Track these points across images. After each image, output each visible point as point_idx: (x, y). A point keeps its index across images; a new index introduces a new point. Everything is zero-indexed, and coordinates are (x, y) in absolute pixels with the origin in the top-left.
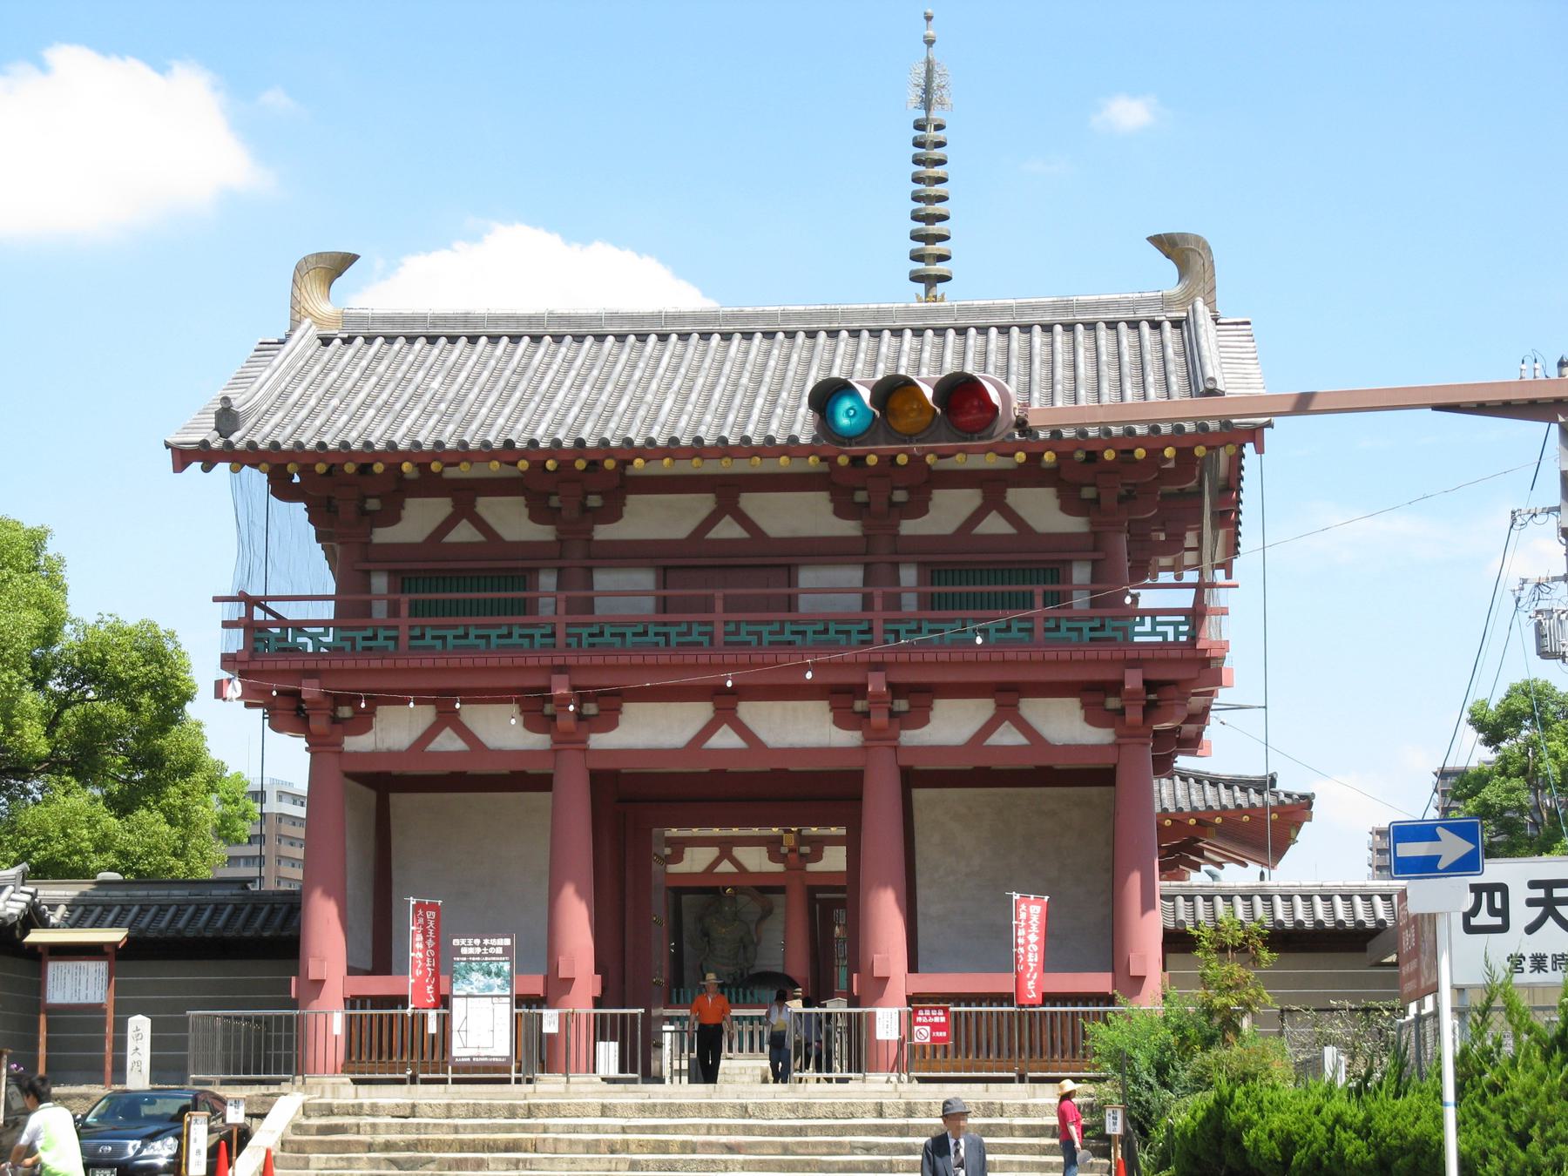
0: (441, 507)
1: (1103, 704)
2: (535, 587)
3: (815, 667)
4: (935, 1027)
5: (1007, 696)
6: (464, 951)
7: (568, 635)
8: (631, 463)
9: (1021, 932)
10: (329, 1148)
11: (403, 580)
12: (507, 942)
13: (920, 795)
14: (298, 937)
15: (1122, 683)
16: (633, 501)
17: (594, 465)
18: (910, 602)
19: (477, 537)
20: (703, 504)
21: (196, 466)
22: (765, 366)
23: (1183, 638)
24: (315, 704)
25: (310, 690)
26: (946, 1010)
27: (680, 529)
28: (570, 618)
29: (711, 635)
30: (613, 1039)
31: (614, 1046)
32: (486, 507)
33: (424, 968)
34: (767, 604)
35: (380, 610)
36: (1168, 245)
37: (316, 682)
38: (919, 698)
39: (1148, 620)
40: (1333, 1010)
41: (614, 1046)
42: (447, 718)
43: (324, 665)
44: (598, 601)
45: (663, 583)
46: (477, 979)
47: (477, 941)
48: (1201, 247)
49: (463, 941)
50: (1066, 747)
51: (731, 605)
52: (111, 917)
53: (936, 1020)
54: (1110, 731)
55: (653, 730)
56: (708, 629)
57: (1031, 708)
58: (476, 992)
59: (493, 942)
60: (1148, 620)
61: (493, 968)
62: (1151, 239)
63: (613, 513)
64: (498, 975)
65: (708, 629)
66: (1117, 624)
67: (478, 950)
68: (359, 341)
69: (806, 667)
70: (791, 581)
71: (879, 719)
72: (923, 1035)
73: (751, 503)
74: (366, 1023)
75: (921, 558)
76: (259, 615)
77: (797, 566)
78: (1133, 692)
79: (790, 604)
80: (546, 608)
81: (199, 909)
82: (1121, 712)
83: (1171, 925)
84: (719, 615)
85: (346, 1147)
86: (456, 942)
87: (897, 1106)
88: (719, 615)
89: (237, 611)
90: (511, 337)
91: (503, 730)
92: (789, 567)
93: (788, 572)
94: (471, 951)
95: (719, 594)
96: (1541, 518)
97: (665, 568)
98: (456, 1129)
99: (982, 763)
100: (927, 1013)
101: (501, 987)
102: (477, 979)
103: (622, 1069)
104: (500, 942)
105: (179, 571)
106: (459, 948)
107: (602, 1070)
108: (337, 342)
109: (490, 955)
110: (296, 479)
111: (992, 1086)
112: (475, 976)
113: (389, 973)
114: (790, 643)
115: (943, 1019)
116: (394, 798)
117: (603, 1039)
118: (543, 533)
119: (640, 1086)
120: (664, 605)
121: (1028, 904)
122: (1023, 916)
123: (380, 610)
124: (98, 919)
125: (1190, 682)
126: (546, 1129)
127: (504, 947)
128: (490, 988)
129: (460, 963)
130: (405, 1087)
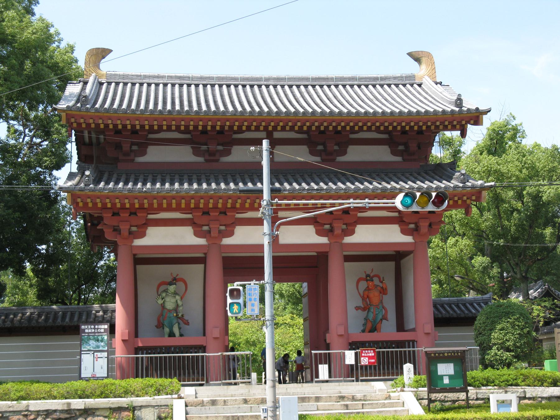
4: (370, 358)
6: (87, 331)
12: (106, 327)
13: (139, 267)
26: (374, 350)
30: (325, 363)
31: (326, 367)
41: (326, 367)
46: (93, 343)
47: (93, 327)
48: (429, 55)
49: (86, 327)
53: (370, 355)
54: (205, 239)
58: (92, 349)
59: (100, 327)
61: (100, 338)
64: (102, 341)
67: (93, 330)
71: (214, 233)
72: (364, 361)
82: (209, 232)
86: (83, 327)
94: (90, 331)
100: (367, 351)
103: (330, 376)
104: (103, 327)
106: (84, 330)
115: (373, 354)
117: (321, 363)
119: (355, 383)
127: (105, 329)
128: (98, 347)
129: (85, 336)
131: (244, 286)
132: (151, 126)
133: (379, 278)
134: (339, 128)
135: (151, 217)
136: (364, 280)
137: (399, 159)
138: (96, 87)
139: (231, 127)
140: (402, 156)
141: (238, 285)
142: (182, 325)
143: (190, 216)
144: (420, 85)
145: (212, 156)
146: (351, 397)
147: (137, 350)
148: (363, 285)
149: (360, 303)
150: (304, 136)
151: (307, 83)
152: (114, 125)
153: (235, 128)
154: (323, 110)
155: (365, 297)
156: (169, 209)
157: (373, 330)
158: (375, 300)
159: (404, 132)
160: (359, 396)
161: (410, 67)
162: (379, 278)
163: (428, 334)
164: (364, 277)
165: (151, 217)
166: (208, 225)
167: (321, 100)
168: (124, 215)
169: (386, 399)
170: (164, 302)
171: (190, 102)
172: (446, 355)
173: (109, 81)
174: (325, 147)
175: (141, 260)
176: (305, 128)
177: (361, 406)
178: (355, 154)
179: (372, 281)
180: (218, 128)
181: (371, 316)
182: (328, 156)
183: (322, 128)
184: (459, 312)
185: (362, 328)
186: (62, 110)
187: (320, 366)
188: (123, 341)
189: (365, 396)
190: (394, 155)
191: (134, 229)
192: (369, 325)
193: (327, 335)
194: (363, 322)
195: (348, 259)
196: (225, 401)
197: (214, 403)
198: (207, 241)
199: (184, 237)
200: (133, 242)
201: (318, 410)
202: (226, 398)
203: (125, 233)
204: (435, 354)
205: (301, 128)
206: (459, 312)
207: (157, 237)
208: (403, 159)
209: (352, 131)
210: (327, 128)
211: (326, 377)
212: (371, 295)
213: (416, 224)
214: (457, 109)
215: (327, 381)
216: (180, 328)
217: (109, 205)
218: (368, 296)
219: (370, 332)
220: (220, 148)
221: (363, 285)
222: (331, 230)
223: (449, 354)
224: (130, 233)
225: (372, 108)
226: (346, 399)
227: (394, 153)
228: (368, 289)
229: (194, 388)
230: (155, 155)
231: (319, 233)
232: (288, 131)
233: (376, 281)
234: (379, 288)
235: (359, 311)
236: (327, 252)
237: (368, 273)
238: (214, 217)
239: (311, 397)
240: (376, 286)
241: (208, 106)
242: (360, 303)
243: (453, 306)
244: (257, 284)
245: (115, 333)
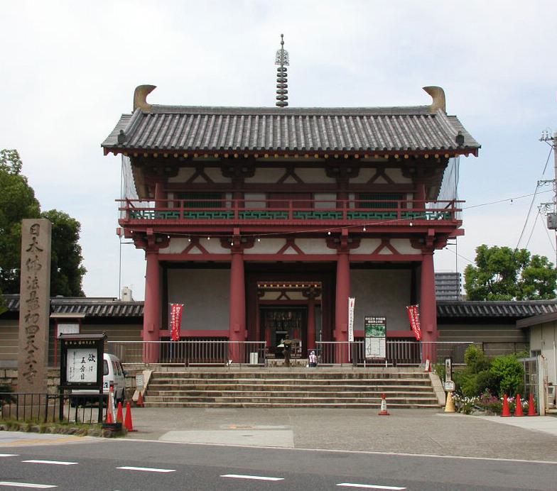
0: (192, 171)
1: (333, 241)
2: (225, 198)
3: (366, 227)
5: (290, 239)
6: (369, 322)
7: (348, 215)
8: (193, 156)
9: (173, 316)
10: (164, 388)
11: (179, 195)
15: (341, 233)
16: (258, 170)
17: (351, 157)
18: (352, 205)
19: (385, 182)
20: (282, 172)
21: (111, 154)
22: (184, 125)
23: (153, 218)
24: (150, 236)
25: (150, 232)
27: (274, 181)
28: (240, 209)
29: (288, 215)
32: (208, 171)
33: (175, 327)
34: (304, 205)
35: (171, 206)
36: (430, 90)
37: (152, 229)
38: (356, 238)
39: (435, 212)
42: (195, 242)
43: (155, 223)
44: (246, 204)
45: (268, 198)
46: (374, 331)
48: (441, 91)
50: (405, 255)
51: (295, 205)
52: (72, 310)
55: (265, 249)
56: (287, 213)
57: (394, 243)
59: (379, 319)
60: (435, 212)
61: (379, 328)
62: (425, 88)
63: (251, 174)
64: (381, 330)
65: (287, 213)
66: (270, 213)
68: (156, 115)
69: (363, 227)
70: (312, 197)
73: (298, 171)
74: (427, 345)
75: (176, 190)
76: (130, 206)
77: (315, 193)
78: (345, 237)
79: (312, 205)
80: (229, 205)
81: (102, 307)
83: (439, 316)
84: (291, 208)
85: (170, 388)
87: (356, 375)
88: (291, 208)
89: (119, 204)
91: (215, 248)
92: (311, 193)
93: (311, 195)
95: (291, 201)
96: (547, 183)
97: (270, 193)
98: (207, 382)
101: (382, 334)
102: (374, 331)
104: (382, 319)
105: (86, 188)
107: (252, 363)
108: (149, 115)
111: (201, 368)
112: (373, 331)
113: (438, 323)
114: (315, 218)
116: (169, 270)
118: (227, 180)
120: (269, 205)
121: (176, 307)
122: (174, 311)
123: (171, 206)
124: (67, 310)
125: (449, 233)
126: (238, 382)
130: (184, 368)
144: (433, 116)
161: (427, 101)
163: (430, 333)
170: (50, 314)
172: (80, 343)
187: (252, 354)
188: (150, 332)
193: (334, 331)
204: (69, 342)
211: (256, 363)
215: (256, 366)
223: (84, 343)
243: (459, 307)
245: (19, 319)
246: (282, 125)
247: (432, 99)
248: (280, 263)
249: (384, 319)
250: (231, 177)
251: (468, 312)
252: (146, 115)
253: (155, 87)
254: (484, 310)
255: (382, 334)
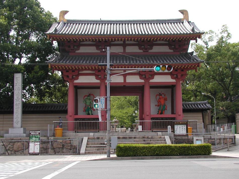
14: (23, 114)
40: (206, 87)
46: (34, 138)
54: (99, 80)
61: (37, 137)
62: (180, 11)
64: (38, 138)
67: (34, 133)
90: (73, 23)
94: (33, 134)
99: (188, 11)
101: (38, 140)
103: (142, 130)
104: (38, 132)
109: (36, 134)
110: (17, 54)
112: (34, 138)
127: (39, 133)
128: (36, 140)
131: (100, 98)
132: (112, 40)
133: (164, 94)
134: (180, 39)
135: (80, 72)
136: (158, 95)
137: (172, 51)
138: (62, 25)
139: (153, 39)
140: (173, 50)
141: (97, 98)
142: (92, 111)
143: (94, 72)
145: (146, 50)
146: (147, 137)
147: (76, 119)
148: (158, 97)
149: (157, 104)
150: (137, 43)
151: (171, 22)
152: (79, 40)
153: (155, 40)
154: (184, 33)
155: (159, 101)
156: (86, 69)
157: (162, 113)
158: (162, 103)
159: (70, 41)
160: (150, 137)
161: (181, 16)
162: (164, 94)
163: (148, 115)
164: (159, 94)
165: (80, 72)
166: (145, 75)
167: (159, 29)
168: (179, 71)
169: (160, 138)
171: (132, 32)
173: (68, 22)
174: (175, 46)
175: (77, 88)
176: (167, 40)
177: (150, 141)
178: (156, 49)
179: (161, 95)
180: (148, 40)
181: (161, 109)
182: (146, 50)
183: (174, 40)
184: (191, 107)
185: (158, 113)
186: (48, 34)
189: (152, 137)
190: (170, 49)
191: (74, 77)
192: (160, 111)
194: (158, 110)
195: (152, 87)
196: (102, 138)
197: (98, 138)
198: (144, 81)
199: (92, 80)
200: (74, 81)
201: (134, 141)
202: (102, 137)
203: (70, 77)
205: (166, 39)
206: (188, 107)
207: (82, 80)
208: (174, 51)
209: (156, 40)
210: (175, 39)
212: (161, 101)
213: (177, 75)
214: (192, 32)
216: (91, 112)
217: (97, 69)
218: (160, 101)
219: (160, 114)
220: (149, 47)
221: (158, 97)
222: (177, 77)
224: (73, 78)
225: (186, 32)
226: (145, 138)
227: (170, 49)
228: (160, 98)
229: (93, 133)
230: (83, 50)
231: (172, 78)
232: (88, 41)
233: (163, 95)
234: (164, 98)
235: (156, 106)
236: (100, 87)
237: (160, 93)
238: (100, 72)
239: (133, 137)
240: (163, 97)
241: (126, 32)
242: (157, 104)
243: (193, 105)
244: (104, 98)
245: (13, 114)
246: (128, 27)
247: (183, 15)
248: (124, 86)
249: (39, 132)
250: (100, 50)
251: (200, 107)
252: (65, 24)
253: (68, 11)
254: (203, 106)
255: (38, 140)
